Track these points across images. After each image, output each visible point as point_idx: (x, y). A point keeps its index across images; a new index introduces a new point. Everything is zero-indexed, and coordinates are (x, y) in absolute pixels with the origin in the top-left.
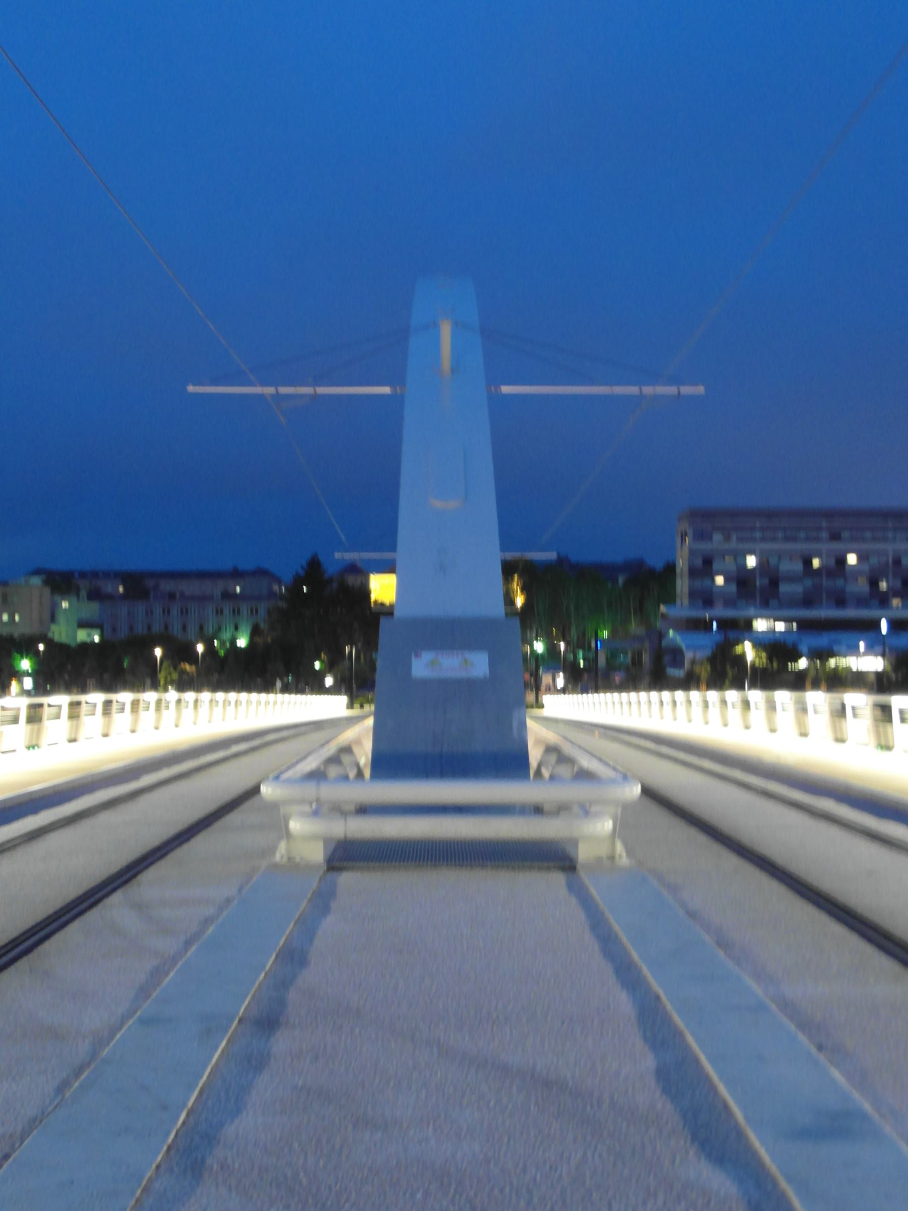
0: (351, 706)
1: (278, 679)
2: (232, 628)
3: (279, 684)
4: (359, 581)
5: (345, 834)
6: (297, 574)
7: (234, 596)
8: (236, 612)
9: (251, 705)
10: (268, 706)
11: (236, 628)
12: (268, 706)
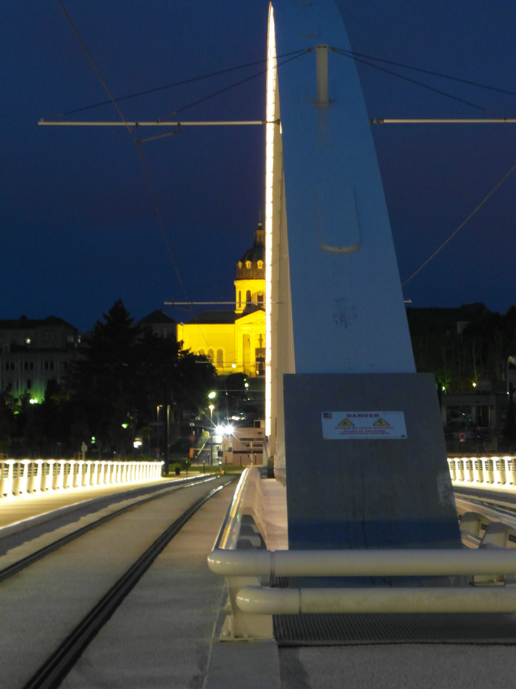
0: (165, 472)
1: (83, 443)
2: (25, 386)
3: (84, 448)
4: (165, 333)
5: (300, 609)
6: (99, 323)
7: (25, 348)
8: (29, 366)
9: (78, 473)
10: (20, 478)
11: (29, 385)
12: (20, 478)
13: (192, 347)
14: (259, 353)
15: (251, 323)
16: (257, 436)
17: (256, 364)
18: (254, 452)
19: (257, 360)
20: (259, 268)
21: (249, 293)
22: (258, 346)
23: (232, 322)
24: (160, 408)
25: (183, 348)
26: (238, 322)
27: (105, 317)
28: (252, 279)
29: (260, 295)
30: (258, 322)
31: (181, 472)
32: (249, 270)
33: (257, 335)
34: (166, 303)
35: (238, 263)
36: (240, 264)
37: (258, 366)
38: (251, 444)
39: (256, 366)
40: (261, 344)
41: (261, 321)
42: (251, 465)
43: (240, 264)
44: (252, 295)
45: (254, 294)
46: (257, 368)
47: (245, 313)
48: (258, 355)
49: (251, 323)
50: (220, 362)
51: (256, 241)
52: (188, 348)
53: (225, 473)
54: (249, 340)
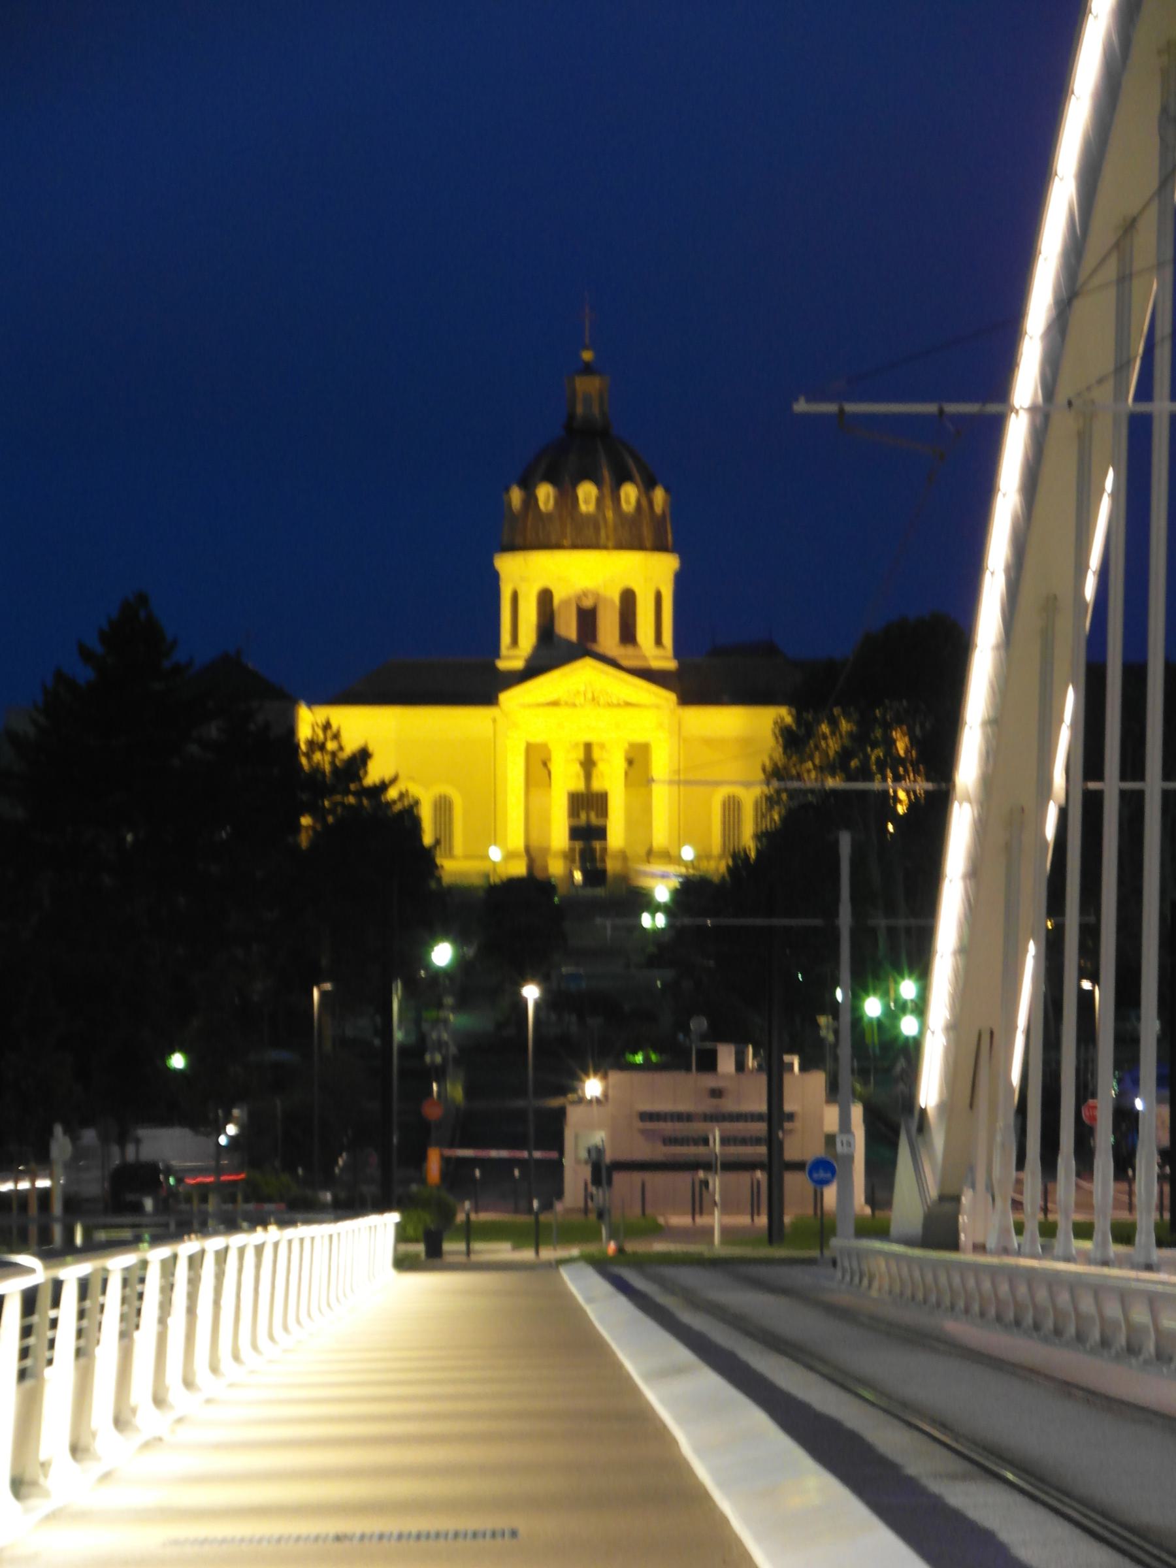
1: (58, 1130)
6: (59, 676)
13: (400, 774)
14: (583, 809)
15: (555, 704)
16: (707, 1105)
17: (572, 850)
18: (731, 1166)
19: (576, 833)
20: (583, 508)
21: (545, 597)
22: (579, 785)
23: (487, 697)
24: (323, 994)
25: (366, 773)
26: (510, 698)
27: (86, 655)
28: (558, 546)
29: (588, 603)
30: (580, 700)
31: (447, 1246)
32: (549, 516)
33: (577, 745)
34: (801, 406)
35: (507, 489)
36: (516, 496)
37: (577, 857)
38: (717, 1134)
39: (568, 856)
40: (588, 777)
41: (589, 696)
42: (1114, 1252)
43: (516, 496)
44: (559, 607)
45: (566, 603)
46: (573, 861)
47: (534, 669)
48: (578, 816)
49: (555, 704)
50: (443, 838)
51: (571, 416)
52: (388, 775)
53: (620, 1250)
54: (545, 764)
